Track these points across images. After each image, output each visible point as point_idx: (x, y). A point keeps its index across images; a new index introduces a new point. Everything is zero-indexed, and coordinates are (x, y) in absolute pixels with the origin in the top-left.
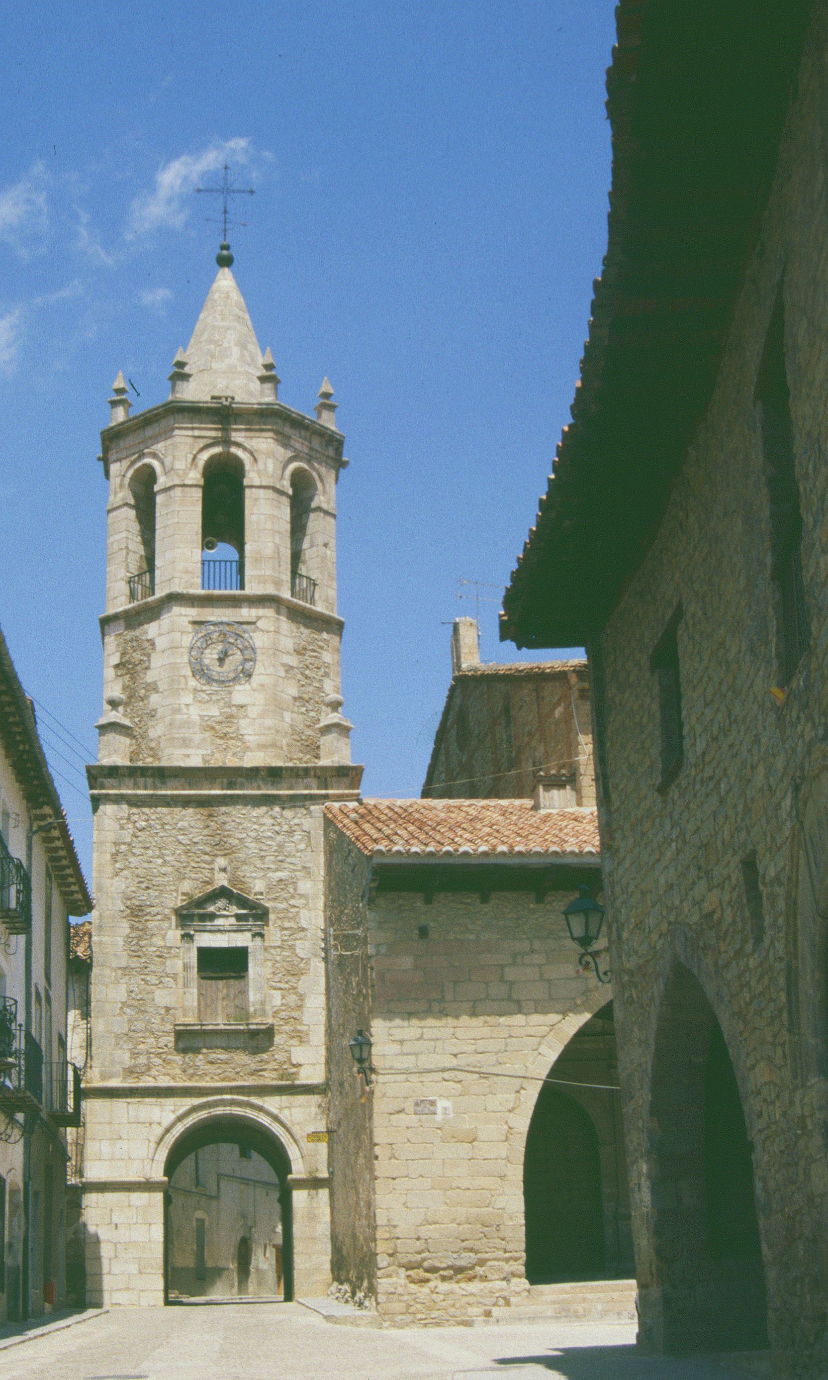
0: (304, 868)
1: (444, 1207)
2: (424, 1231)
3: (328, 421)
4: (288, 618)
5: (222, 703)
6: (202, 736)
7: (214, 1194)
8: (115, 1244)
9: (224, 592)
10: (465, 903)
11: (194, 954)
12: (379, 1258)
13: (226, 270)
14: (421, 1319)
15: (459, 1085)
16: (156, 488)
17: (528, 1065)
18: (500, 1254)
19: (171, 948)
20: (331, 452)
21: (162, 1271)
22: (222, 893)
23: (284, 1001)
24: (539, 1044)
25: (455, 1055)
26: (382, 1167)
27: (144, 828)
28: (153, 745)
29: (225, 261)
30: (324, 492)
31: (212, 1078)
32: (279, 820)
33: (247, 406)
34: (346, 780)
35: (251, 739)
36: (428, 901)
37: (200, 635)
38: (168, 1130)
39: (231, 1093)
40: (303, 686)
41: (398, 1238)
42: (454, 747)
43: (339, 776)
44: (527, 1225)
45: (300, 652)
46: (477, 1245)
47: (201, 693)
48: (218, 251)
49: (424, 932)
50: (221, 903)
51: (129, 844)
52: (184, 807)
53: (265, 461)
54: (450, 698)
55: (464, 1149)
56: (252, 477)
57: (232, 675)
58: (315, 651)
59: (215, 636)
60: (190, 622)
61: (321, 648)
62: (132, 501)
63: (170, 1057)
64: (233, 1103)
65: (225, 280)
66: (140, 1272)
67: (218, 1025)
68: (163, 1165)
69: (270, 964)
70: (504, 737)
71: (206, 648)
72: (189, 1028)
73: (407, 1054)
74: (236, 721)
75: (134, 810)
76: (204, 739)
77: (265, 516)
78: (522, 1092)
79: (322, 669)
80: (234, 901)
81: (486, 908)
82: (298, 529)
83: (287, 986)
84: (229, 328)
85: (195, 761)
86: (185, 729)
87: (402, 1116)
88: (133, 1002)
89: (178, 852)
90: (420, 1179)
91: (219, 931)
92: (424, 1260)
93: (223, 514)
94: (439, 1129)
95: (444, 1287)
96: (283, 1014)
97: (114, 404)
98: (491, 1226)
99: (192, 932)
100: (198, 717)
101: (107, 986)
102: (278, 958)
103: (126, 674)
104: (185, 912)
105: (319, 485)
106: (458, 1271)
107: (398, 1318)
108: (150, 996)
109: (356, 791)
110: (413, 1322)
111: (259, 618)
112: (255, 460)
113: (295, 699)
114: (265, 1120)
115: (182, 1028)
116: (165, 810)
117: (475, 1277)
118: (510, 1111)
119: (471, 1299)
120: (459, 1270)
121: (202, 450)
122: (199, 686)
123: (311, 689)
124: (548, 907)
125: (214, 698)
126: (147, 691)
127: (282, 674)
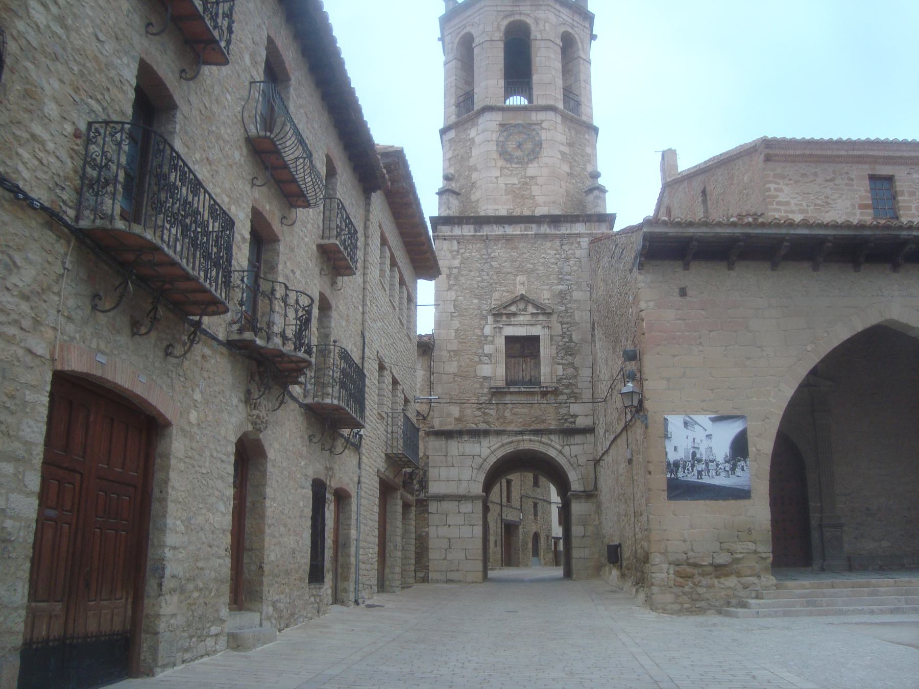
7: (491, 574)
16: (474, 45)
21: (481, 558)
35: (540, 199)
45: (570, 145)
50: (522, 305)
56: (535, 33)
78: (767, 421)
85: (503, 212)
95: (705, 581)
106: (720, 570)
111: (543, 121)
117: (731, 574)
120: (717, 567)
123: (578, 169)
127: (560, 157)
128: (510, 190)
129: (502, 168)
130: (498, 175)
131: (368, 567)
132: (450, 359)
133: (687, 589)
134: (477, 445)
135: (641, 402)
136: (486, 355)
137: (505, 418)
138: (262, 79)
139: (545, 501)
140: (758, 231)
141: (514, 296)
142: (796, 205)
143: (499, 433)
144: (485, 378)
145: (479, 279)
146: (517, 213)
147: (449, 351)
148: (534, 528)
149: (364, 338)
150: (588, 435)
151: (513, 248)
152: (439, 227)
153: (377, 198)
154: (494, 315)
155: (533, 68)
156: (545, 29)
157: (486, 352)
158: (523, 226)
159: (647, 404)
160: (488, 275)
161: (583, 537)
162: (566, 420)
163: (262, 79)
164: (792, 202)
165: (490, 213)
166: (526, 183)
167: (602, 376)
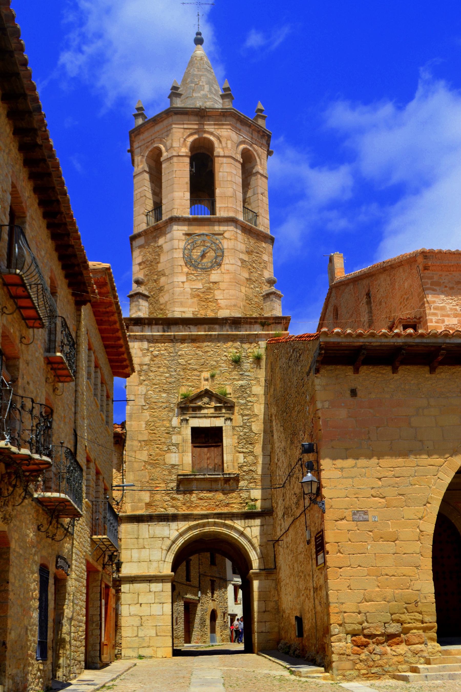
0: (256, 378)
1: (378, 589)
2: (365, 606)
4: (242, 232)
5: (204, 281)
6: (193, 300)
8: (141, 616)
10: (382, 374)
11: (189, 432)
12: (332, 627)
13: (200, 46)
15: (383, 500)
16: (162, 159)
17: (431, 486)
18: (419, 625)
19: (175, 427)
20: (264, 142)
22: (207, 393)
23: (245, 460)
24: (438, 471)
25: (380, 479)
27: (157, 356)
28: (162, 307)
30: (261, 163)
31: (202, 509)
32: (240, 350)
34: (279, 326)
35: (222, 303)
36: (356, 371)
37: (190, 242)
38: (174, 542)
39: (213, 518)
40: (252, 272)
41: (345, 612)
44: (437, 602)
45: (249, 253)
46: (404, 617)
47: (191, 275)
48: (195, 36)
49: (354, 393)
50: (206, 400)
51: (148, 365)
52: (182, 343)
53: (227, 142)
55: (390, 547)
56: (218, 150)
57: (210, 265)
58: (258, 253)
59: (199, 242)
60: (183, 234)
62: (147, 169)
63: (174, 496)
64: (215, 524)
66: (157, 636)
68: (171, 564)
69: (236, 437)
71: (193, 249)
72: (186, 477)
73: (346, 478)
74: (212, 291)
75: (152, 345)
76: (193, 302)
77: (227, 175)
78: (428, 505)
79: (263, 264)
80: (214, 399)
81: (396, 376)
82: (246, 185)
83: (246, 450)
84: (202, 75)
85: (189, 315)
86: (182, 297)
87: (344, 521)
88: (151, 461)
89: (178, 369)
90: (359, 568)
91: (205, 417)
92: (363, 629)
93: (203, 185)
94: (371, 531)
95: (379, 649)
96: (245, 468)
97: (136, 116)
98: (412, 605)
99: (188, 418)
100: (189, 289)
101: (135, 452)
102: (241, 434)
103: (146, 267)
104: (183, 406)
105: (258, 160)
106: (390, 638)
107: (348, 673)
108: (162, 458)
111: (225, 231)
112: (220, 141)
113: (247, 279)
114: (235, 535)
115: (182, 477)
116: (170, 345)
117: (402, 642)
118: (420, 519)
119: (401, 658)
121: (189, 136)
122: (190, 272)
123: (256, 275)
124: (438, 376)
125: (199, 278)
126: (158, 276)
127: (240, 264)
128: (195, 294)
129: (188, 274)
130: (185, 280)
131: (78, 643)
132: (141, 449)
133: (363, 657)
134: (166, 528)
135: (319, 489)
136: (173, 445)
137: (192, 502)
138: (7, 224)
139: (221, 579)
140: (418, 340)
141: (199, 391)
142: (451, 309)
143: (186, 517)
144: (173, 466)
145: (167, 375)
146: (202, 314)
147: (140, 441)
149: (76, 435)
150: (267, 517)
151: (198, 347)
152: (130, 327)
153: (86, 310)
154: (181, 408)
155: (217, 183)
156: (227, 147)
157: (174, 441)
158: (207, 327)
159: (324, 492)
160: (175, 371)
161: (264, 612)
162: (247, 503)
163: (7, 224)
164: (448, 307)
165: (177, 315)
166: (210, 288)
167: (280, 464)
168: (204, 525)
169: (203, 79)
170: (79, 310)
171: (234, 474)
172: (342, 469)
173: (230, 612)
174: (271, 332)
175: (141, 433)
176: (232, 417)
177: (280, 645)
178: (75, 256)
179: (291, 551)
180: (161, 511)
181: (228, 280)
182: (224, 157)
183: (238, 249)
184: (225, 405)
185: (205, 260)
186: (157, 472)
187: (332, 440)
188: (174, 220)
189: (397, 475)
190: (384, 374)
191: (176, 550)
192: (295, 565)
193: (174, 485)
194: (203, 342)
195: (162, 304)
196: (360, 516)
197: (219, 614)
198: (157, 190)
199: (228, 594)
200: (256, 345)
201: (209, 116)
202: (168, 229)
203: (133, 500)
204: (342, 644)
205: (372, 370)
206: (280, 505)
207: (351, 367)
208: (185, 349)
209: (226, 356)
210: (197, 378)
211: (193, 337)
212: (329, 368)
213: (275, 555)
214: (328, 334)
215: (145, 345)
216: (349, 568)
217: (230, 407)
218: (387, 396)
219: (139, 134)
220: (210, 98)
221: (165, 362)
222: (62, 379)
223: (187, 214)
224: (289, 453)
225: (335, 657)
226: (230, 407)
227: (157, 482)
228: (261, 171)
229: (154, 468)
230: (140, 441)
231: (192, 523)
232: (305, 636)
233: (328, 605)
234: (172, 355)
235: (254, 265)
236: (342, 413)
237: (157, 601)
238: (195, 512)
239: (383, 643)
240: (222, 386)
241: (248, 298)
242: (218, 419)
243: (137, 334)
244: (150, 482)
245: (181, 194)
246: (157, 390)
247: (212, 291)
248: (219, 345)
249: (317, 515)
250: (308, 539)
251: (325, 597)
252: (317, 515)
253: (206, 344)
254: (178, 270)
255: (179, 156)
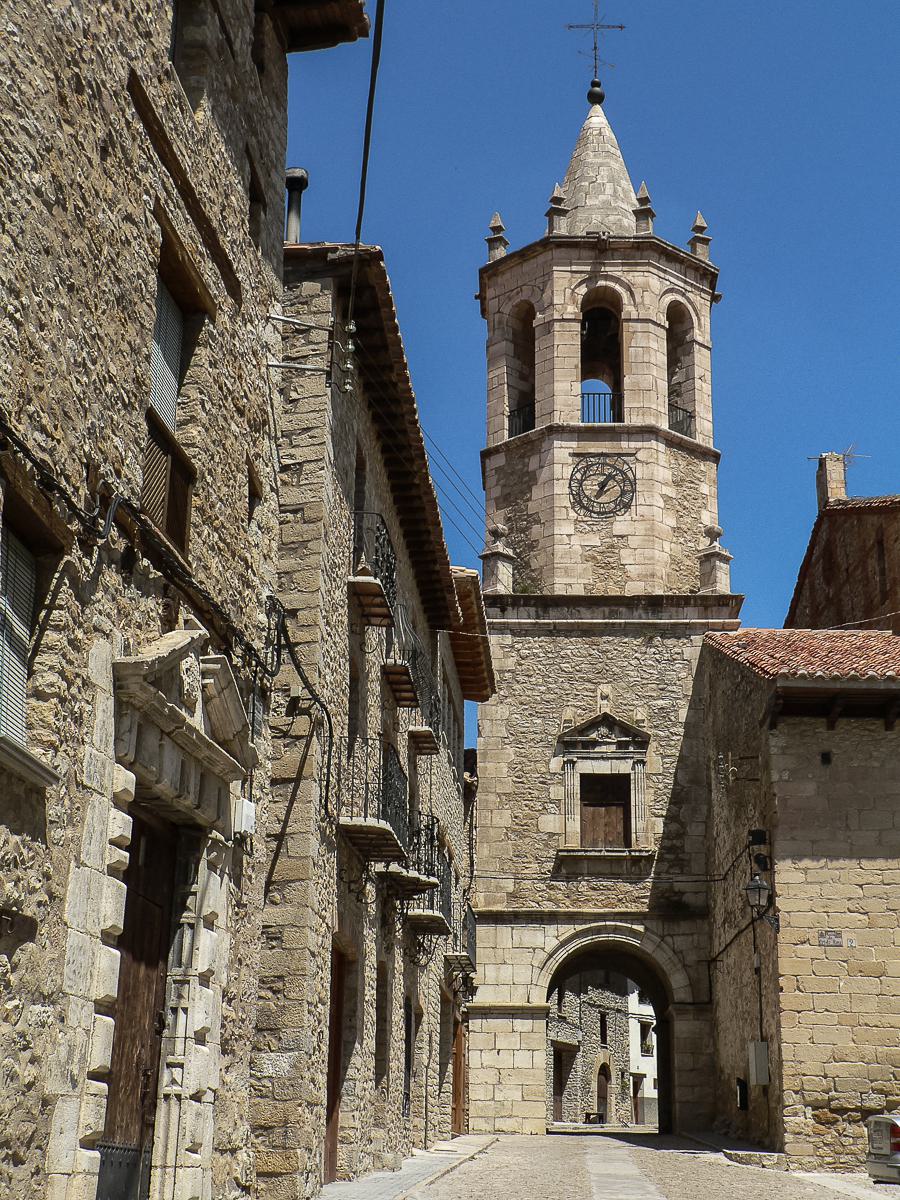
1: (853, 1044)
2: (833, 1068)
3: (702, 254)
5: (602, 534)
6: (584, 566)
9: (610, 422)
10: (869, 730)
14: (830, 1164)
15: (865, 917)
22: (606, 720)
26: (787, 999)
29: (595, 98)
30: (699, 324)
33: (232, 814)
34: (726, 610)
35: (632, 570)
36: (831, 726)
38: (551, 956)
40: (682, 516)
41: (804, 1075)
42: (819, 581)
43: (719, 605)
45: (677, 484)
47: (582, 524)
49: (826, 758)
53: (647, 292)
54: (815, 532)
55: (872, 985)
56: (628, 309)
61: (699, 479)
64: (616, 930)
65: (598, 118)
67: (601, 851)
69: (652, 791)
70: (877, 569)
72: (572, 854)
73: (811, 883)
74: (617, 551)
77: (645, 351)
84: (601, 165)
85: (578, 590)
87: (807, 946)
88: (517, 827)
90: (826, 1013)
91: (603, 758)
92: (831, 1100)
93: (603, 349)
94: (844, 961)
99: (575, 759)
102: (660, 786)
104: (566, 739)
105: (694, 318)
109: (737, 620)
110: (821, 1166)
123: (689, 520)
125: (595, 528)
127: (662, 505)
128: (590, 556)
134: (540, 935)
135: (771, 899)
139: (619, 1011)
143: (571, 918)
144: (551, 835)
145: (543, 689)
146: (599, 590)
147: (499, 795)
148: (600, 1057)
153: (442, 636)
155: (626, 370)
159: (779, 902)
161: (692, 1070)
166: (613, 546)
168: (598, 931)
169: (604, 171)
170: (433, 636)
171: (648, 851)
172: (806, 870)
173: (633, 1070)
174: (710, 621)
175: (501, 782)
176: (645, 760)
177: (716, 1123)
178: (439, 581)
179: (734, 979)
180: (533, 907)
181: (643, 532)
182: (637, 320)
183: (660, 479)
184: (635, 739)
185: (603, 499)
186: (525, 845)
187: (792, 829)
188: (556, 431)
189: (885, 882)
190: (873, 731)
191: (554, 968)
192: (739, 1001)
193: (550, 865)
194: (601, 635)
195: (533, 571)
196: (829, 938)
197: (614, 1074)
198: (526, 371)
199: (630, 1038)
200: (685, 641)
201: (613, 249)
202: (545, 445)
203: (488, 888)
204: (800, 1119)
205: (854, 725)
206: (718, 905)
207: (824, 720)
208: (572, 646)
209: (638, 660)
210: (591, 694)
211: (585, 628)
212: (791, 720)
213: (710, 982)
214: (788, 677)
215: (508, 639)
216: (811, 1013)
217: (642, 742)
218: (876, 764)
219: (495, 275)
220: (615, 209)
221: (540, 666)
222: (424, 751)
223: (577, 423)
224: (733, 830)
225: (788, 1137)
226: (642, 742)
227: (526, 860)
228: (699, 339)
229: (521, 838)
230: (499, 795)
231: (579, 928)
232: (751, 1108)
233: (780, 1063)
234: (550, 655)
235: (685, 503)
236: (810, 788)
237: (524, 1046)
238: (586, 910)
239: (858, 1121)
240: (631, 708)
241: (674, 560)
242: (623, 761)
243: (495, 621)
244: (515, 859)
245: (567, 386)
246: (527, 713)
247: (617, 551)
248: (626, 640)
249: (769, 933)
250: (755, 966)
251: (777, 1053)
252: (769, 933)
253: (605, 638)
254: (560, 514)
255: (563, 320)
